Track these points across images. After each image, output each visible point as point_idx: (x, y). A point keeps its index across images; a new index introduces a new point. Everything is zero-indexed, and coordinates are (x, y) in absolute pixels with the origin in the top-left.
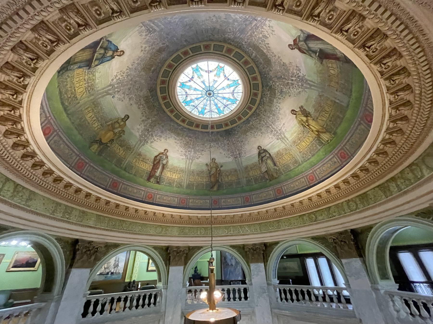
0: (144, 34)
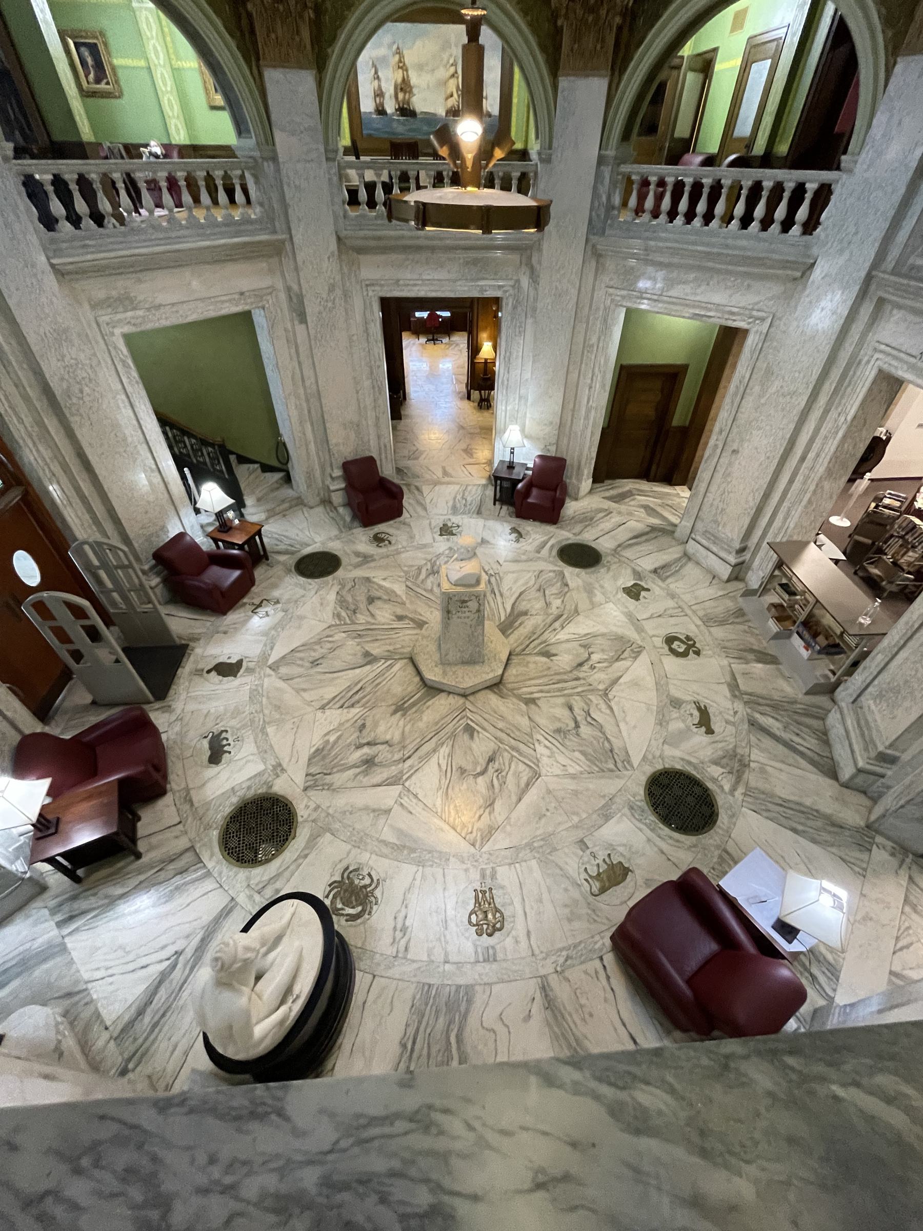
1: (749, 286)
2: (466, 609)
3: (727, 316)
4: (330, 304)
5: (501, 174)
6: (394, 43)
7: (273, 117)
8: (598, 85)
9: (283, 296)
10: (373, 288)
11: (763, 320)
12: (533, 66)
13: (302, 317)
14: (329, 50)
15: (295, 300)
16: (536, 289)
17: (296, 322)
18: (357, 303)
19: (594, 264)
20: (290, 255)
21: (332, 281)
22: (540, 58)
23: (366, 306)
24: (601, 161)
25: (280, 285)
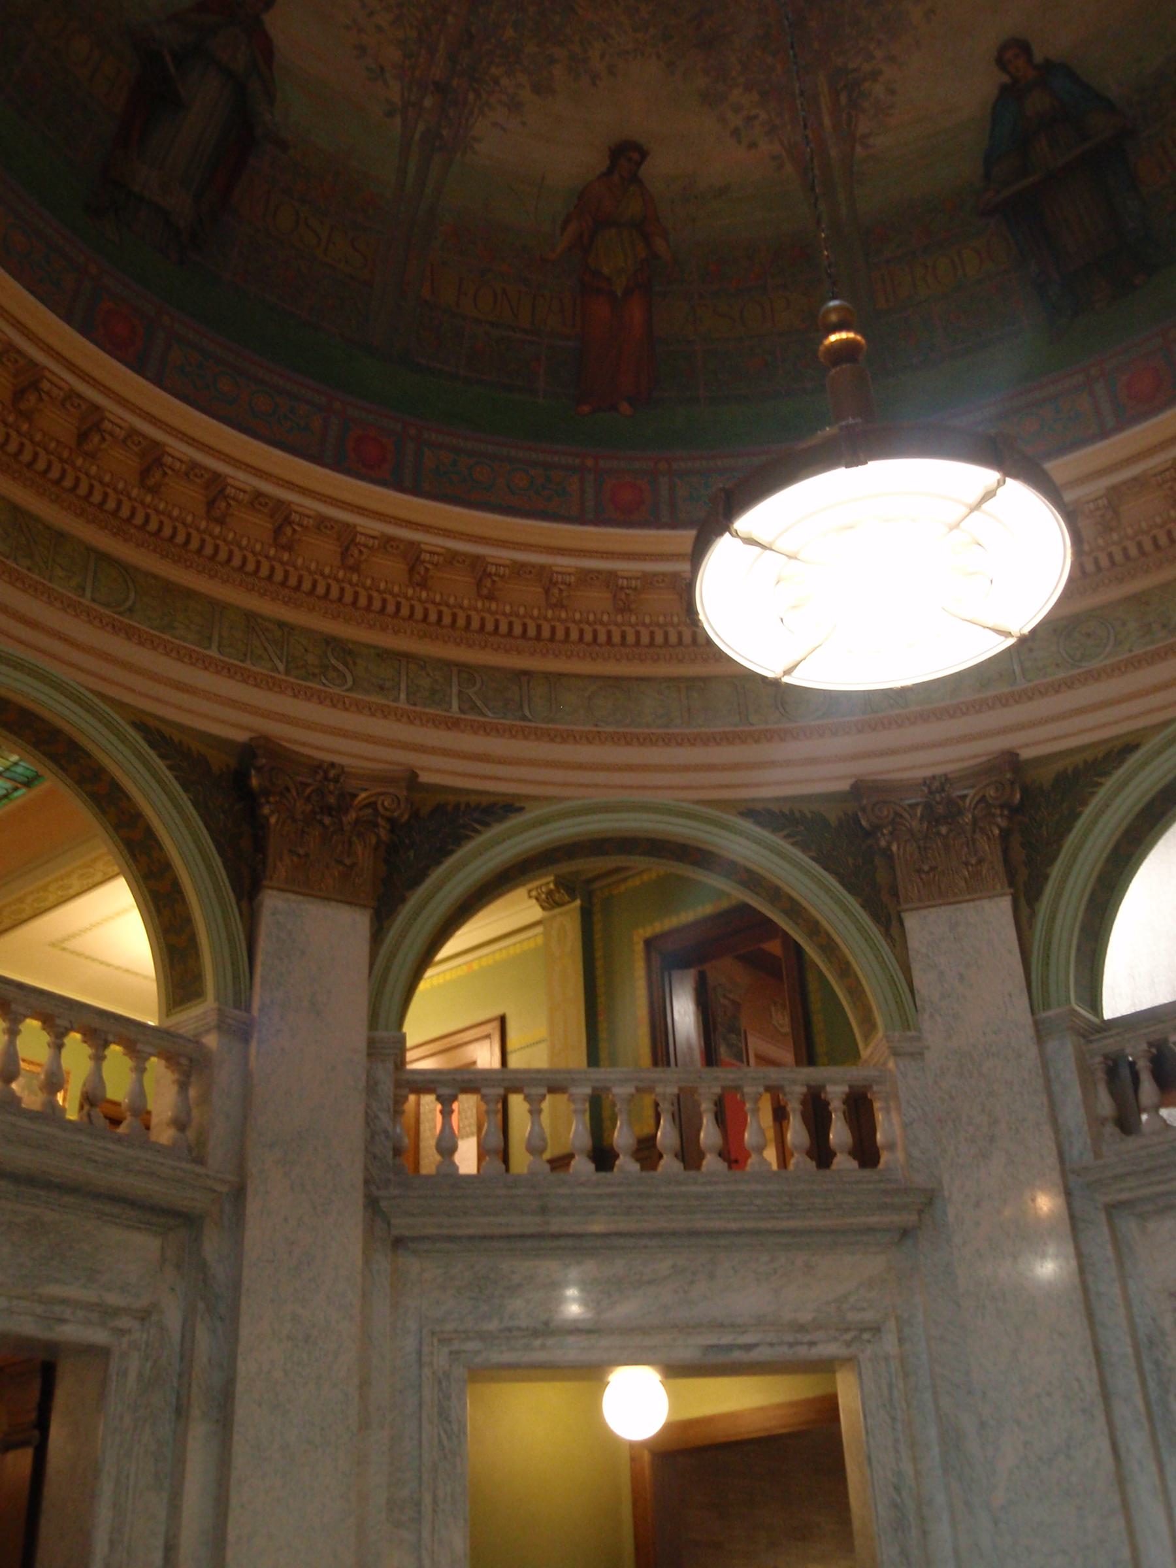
0: (878, 89)
3: (789, 1338)
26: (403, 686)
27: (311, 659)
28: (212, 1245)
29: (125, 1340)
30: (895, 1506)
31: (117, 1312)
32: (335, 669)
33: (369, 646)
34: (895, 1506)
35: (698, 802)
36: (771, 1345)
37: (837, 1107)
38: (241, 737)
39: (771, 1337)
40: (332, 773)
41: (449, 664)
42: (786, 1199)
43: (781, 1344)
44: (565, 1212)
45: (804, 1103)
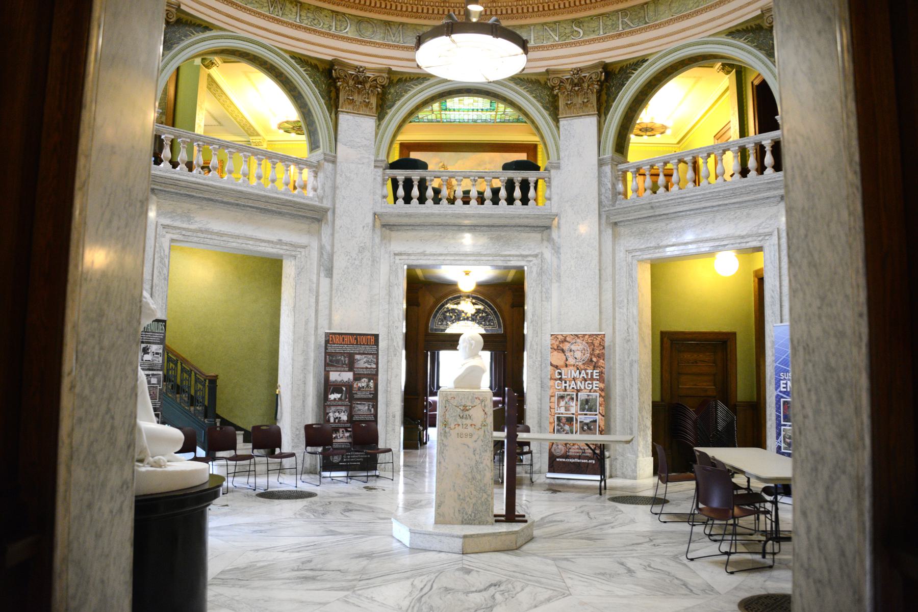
1: (748, 214)
2: (468, 422)
3: (738, 241)
4: (357, 262)
5: (520, 179)
6: (441, 162)
7: (339, 137)
8: (592, 121)
9: (315, 254)
10: (400, 257)
11: (770, 234)
12: (546, 125)
13: (330, 272)
14: (388, 111)
15: (325, 256)
16: (559, 258)
17: (322, 275)
18: (384, 268)
19: (610, 231)
20: (330, 223)
21: (362, 245)
22: (545, 113)
23: (393, 271)
24: (601, 163)
25: (315, 245)
26: (601, 27)
27: (567, 31)
28: (554, 234)
29: (531, 263)
30: (772, 297)
31: (527, 256)
32: (576, 31)
33: (587, 17)
34: (772, 297)
35: (710, 36)
36: (732, 244)
37: (768, 149)
38: (330, 58)
39: (732, 241)
40: (361, 69)
41: (617, 11)
42: (731, 192)
43: (736, 243)
44: (659, 207)
45: (404, 182)
